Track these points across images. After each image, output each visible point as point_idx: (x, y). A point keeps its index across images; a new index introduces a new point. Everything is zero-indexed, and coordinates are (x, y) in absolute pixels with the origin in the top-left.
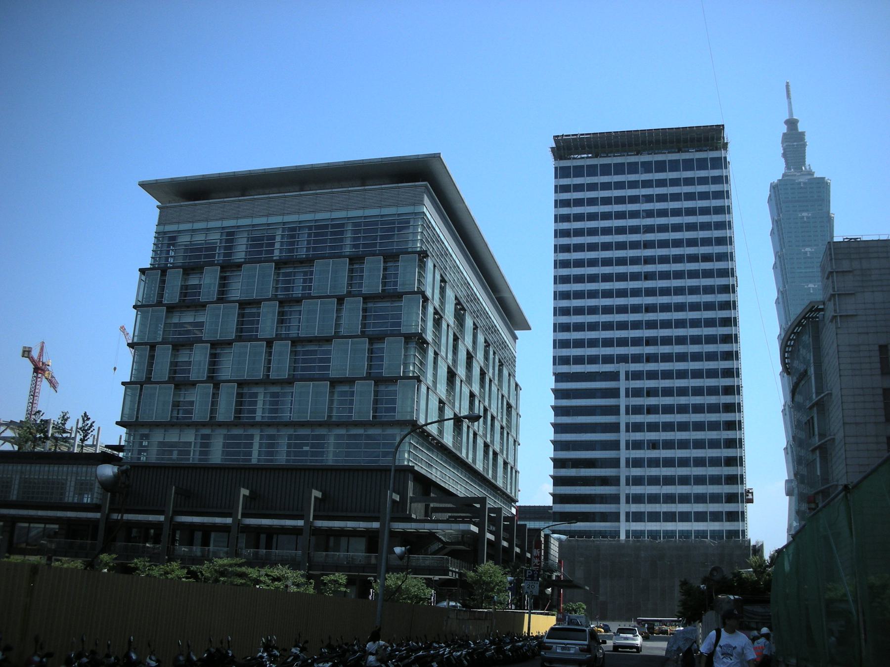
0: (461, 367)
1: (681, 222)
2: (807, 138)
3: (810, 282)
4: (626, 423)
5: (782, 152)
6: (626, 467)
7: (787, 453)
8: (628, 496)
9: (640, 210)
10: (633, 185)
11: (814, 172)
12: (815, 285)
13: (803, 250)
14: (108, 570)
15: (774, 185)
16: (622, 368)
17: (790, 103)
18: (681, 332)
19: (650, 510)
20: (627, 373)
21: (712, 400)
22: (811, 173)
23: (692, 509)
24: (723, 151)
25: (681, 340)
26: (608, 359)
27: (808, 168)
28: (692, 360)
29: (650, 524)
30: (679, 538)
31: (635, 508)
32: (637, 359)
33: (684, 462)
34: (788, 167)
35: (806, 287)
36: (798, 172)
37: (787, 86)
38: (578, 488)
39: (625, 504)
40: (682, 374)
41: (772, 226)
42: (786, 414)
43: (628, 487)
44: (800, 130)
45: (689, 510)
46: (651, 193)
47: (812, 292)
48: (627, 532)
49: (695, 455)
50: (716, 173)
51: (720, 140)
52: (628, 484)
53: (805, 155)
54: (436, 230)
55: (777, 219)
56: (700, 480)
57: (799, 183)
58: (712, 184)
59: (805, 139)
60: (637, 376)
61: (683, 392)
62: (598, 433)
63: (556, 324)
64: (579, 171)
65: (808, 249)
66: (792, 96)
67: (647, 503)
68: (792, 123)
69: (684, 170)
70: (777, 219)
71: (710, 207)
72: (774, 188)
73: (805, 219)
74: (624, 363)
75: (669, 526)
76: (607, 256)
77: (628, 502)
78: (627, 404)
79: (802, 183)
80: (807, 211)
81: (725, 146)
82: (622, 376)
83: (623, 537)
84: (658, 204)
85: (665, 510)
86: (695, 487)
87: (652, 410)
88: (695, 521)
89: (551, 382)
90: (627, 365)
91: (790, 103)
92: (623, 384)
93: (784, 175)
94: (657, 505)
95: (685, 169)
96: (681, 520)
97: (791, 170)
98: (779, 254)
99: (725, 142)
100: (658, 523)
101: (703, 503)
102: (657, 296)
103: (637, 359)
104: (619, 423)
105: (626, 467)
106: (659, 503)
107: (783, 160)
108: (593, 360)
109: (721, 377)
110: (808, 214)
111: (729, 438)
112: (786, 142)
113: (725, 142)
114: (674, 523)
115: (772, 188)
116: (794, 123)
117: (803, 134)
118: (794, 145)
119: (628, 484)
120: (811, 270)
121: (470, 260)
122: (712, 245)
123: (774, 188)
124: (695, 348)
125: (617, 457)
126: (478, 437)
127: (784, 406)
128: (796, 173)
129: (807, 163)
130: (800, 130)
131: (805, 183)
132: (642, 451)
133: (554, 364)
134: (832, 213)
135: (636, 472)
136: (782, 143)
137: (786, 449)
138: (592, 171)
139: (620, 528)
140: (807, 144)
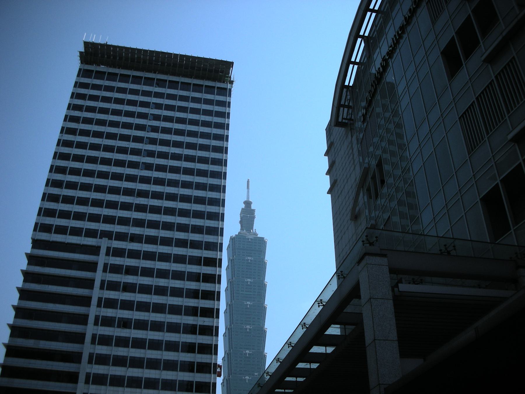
2: (256, 214)
3: (248, 301)
4: (99, 298)
5: (240, 220)
11: (258, 234)
12: (251, 303)
13: (246, 280)
15: (233, 237)
16: (104, 243)
17: (248, 192)
20: (108, 249)
22: (256, 234)
24: (229, 84)
25: (168, 226)
26: (91, 233)
27: (254, 231)
32: (121, 237)
35: (245, 303)
36: (248, 233)
37: (248, 182)
40: (164, 257)
42: (224, 386)
43: (90, 365)
44: (252, 208)
50: (221, 98)
53: (254, 224)
55: (232, 259)
56: (172, 346)
57: (248, 239)
59: (254, 214)
60: (119, 253)
65: (249, 280)
66: (250, 187)
67: (109, 385)
68: (248, 204)
70: (232, 259)
72: (232, 239)
78: (104, 279)
80: (251, 256)
81: (232, 82)
82: (103, 251)
87: (129, 288)
90: (110, 241)
91: (248, 192)
97: (244, 231)
98: (231, 280)
103: (121, 237)
107: (240, 225)
110: (252, 258)
112: (243, 214)
115: (231, 239)
116: (249, 204)
117: (254, 210)
118: (248, 216)
119: (90, 362)
122: (210, 151)
124: (182, 235)
125: (83, 331)
128: (246, 233)
129: (254, 228)
130: (252, 208)
131: (251, 239)
134: (266, 260)
136: (240, 215)
140: (256, 217)
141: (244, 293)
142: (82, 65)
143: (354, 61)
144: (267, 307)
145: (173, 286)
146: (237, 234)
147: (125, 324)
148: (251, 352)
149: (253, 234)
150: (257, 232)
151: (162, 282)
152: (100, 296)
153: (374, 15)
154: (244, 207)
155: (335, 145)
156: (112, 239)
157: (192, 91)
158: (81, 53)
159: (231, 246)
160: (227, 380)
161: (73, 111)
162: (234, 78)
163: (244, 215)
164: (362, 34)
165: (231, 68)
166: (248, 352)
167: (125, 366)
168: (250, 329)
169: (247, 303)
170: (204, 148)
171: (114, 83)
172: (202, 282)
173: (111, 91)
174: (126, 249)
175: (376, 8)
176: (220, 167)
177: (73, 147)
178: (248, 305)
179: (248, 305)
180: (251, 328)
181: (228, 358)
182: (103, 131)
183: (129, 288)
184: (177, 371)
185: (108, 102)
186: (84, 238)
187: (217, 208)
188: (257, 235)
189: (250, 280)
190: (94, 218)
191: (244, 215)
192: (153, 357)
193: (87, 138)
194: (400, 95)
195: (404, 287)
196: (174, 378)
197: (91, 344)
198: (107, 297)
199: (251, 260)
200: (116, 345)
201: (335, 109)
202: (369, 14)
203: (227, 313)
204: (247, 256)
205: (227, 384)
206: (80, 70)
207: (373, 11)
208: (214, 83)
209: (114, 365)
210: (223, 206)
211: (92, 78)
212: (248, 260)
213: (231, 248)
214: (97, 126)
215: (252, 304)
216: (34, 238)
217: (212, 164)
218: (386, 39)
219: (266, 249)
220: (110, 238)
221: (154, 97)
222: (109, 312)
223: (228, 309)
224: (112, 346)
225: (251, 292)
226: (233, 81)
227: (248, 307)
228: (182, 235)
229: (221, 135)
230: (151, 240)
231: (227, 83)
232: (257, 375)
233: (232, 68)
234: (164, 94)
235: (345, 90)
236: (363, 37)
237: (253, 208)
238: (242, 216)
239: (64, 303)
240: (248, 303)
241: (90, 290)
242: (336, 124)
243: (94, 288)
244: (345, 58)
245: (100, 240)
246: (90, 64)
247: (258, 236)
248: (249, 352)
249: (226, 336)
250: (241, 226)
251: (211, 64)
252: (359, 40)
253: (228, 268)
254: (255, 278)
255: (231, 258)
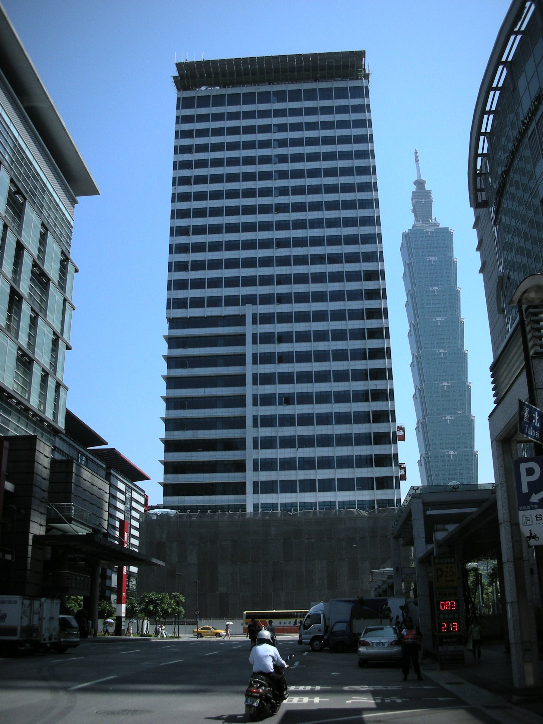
0: (52, 313)
1: (321, 235)
2: (433, 196)
3: (438, 316)
5: (412, 208)
6: (254, 427)
7: (421, 465)
8: (255, 462)
9: (272, 155)
10: (264, 114)
12: (442, 319)
13: (431, 289)
14: (288, 667)
16: (249, 310)
18: (321, 346)
19: (283, 478)
20: (254, 316)
21: (357, 344)
22: (436, 224)
23: (336, 475)
25: (322, 356)
26: (232, 301)
27: (434, 220)
28: (336, 380)
29: (284, 495)
30: (319, 509)
31: (264, 476)
32: (266, 299)
33: (324, 419)
34: (417, 220)
35: (434, 320)
37: (416, 153)
38: (194, 454)
39: (252, 472)
40: (323, 398)
41: (403, 270)
42: (419, 431)
43: (255, 451)
45: (331, 477)
46: (284, 122)
47: (439, 324)
48: (256, 507)
49: (337, 410)
50: (356, 102)
51: (361, 71)
52: (255, 447)
53: (432, 210)
54: (54, 196)
57: (427, 232)
58: (352, 112)
60: (267, 319)
61: (321, 336)
62: (220, 387)
63: (172, 262)
64: (204, 101)
65: (436, 288)
68: (420, 184)
69: (320, 99)
71: (351, 136)
72: (406, 236)
73: (433, 263)
74: (251, 305)
75: (308, 497)
76: (250, 274)
77: (255, 469)
79: (429, 232)
80: (434, 256)
81: (367, 76)
82: (249, 319)
83: (250, 509)
84: (292, 133)
85: (302, 478)
86: (339, 449)
87: (284, 358)
88: (339, 490)
89: (165, 329)
90: (255, 306)
91: (418, 167)
92: (249, 329)
93: (413, 226)
94: (293, 472)
95: (322, 98)
96: (322, 490)
97: (420, 222)
99: (367, 72)
100: (294, 495)
101: (348, 467)
102: (289, 229)
103: (266, 299)
104: (245, 375)
105: (254, 427)
106: (295, 469)
108: (214, 302)
109: (365, 299)
111: (378, 388)
113: (367, 72)
114: (313, 494)
115: (404, 237)
119: (255, 447)
120: (438, 306)
121: (62, 180)
122: (354, 175)
123: (406, 236)
124: (335, 287)
125: (242, 415)
126: (61, 388)
127: (418, 424)
128: (424, 225)
129: (433, 217)
131: (431, 232)
132: (273, 407)
133: (168, 307)
135: (266, 432)
136: (412, 200)
137: (420, 462)
138: (218, 100)
139: (246, 502)
141: (432, 307)
142: (180, 92)
143: (481, 153)
144: (464, 321)
145: (335, 348)
146: (411, 228)
147: (287, 400)
148: (450, 384)
149: (432, 224)
150: (438, 221)
151: (321, 346)
152: (255, 372)
153: (491, 116)
154: (415, 190)
155: (481, 220)
156: (256, 304)
157: (320, 99)
158: (175, 78)
159: (405, 245)
160: (421, 423)
161: (181, 155)
162: (369, 69)
163: (416, 200)
164: (484, 131)
165: (364, 59)
166: (445, 384)
167: (295, 447)
168: (444, 354)
169: (437, 319)
170: (345, 155)
171: (223, 108)
172: (354, 423)
173: (221, 120)
174: (275, 333)
175: (493, 109)
176: (369, 193)
177: (190, 201)
178: (439, 322)
179: (439, 322)
180: (446, 351)
181: (420, 394)
182: (221, 173)
183: (284, 358)
184: (352, 445)
185: (220, 135)
186: (225, 307)
187: (373, 245)
188: (438, 226)
189: (437, 289)
190: (232, 282)
191: (416, 200)
192: (323, 433)
193: (205, 185)
194: (537, 178)
195: (429, 512)
196: (350, 454)
197: (253, 427)
198: (262, 372)
199: (435, 261)
200: (280, 425)
201: (472, 195)
202: (486, 117)
203: (411, 335)
204: (428, 256)
205: (423, 428)
206: (178, 99)
207: (490, 112)
208: (345, 82)
209: (281, 447)
210: (381, 242)
211: (194, 108)
212: (430, 261)
213: (405, 248)
214: (213, 169)
215: (443, 320)
216: (168, 317)
217: (359, 191)
218: (528, 88)
219: (453, 243)
220: (255, 303)
221: (274, 116)
222: (268, 389)
223: (412, 330)
224: (276, 426)
225: (440, 303)
226: (368, 74)
227: (439, 324)
228: (335, 287)
229: (364, 151)
230: (303, 337)
231: (361, 79)
232: (461, 413)
233: (365, 57)
234: (286, 110)
235: (478, 178)
236: (485, 134)
237: (427, 188)
238: (414, 202)
239: (194, 337)
240: (438, 319)
241: (242, 367)
242: (477, 206)
243: (246, 365)
244: (471, 153)
245: (243, 307)
246: (189, 89)
247: (440, 227)
248: (447, 384)
249: (414, 366)
250: (416, 216)
251: (337, 59)
252: (482, 138)
253: (406, 276)
254: (443, 285)
255: (408, 262)
